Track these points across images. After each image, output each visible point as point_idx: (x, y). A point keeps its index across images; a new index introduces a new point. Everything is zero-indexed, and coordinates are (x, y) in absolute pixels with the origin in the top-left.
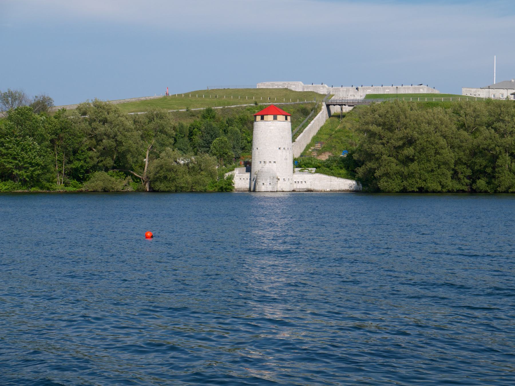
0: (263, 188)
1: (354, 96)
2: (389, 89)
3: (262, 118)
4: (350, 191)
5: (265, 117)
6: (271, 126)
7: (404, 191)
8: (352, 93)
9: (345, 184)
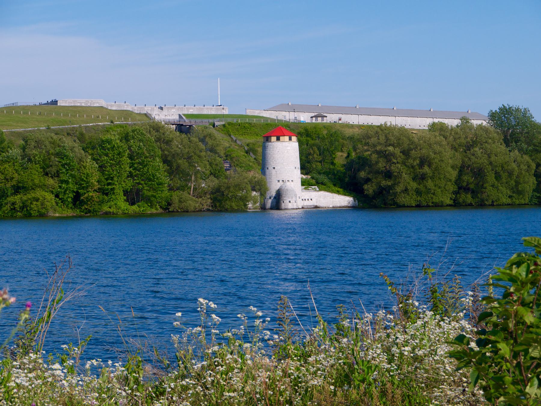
0: (290, 206)
1: (159, 115)
2: (192, 109)
3: (278, 139)
4: (349, 207)
5: (281, 138)
6: (287, 146)
7: (419, 206)
8: (157, 113)
9: (343, 200)
